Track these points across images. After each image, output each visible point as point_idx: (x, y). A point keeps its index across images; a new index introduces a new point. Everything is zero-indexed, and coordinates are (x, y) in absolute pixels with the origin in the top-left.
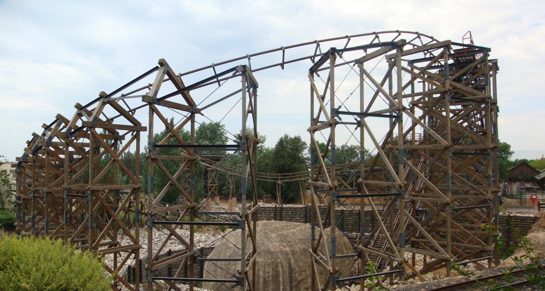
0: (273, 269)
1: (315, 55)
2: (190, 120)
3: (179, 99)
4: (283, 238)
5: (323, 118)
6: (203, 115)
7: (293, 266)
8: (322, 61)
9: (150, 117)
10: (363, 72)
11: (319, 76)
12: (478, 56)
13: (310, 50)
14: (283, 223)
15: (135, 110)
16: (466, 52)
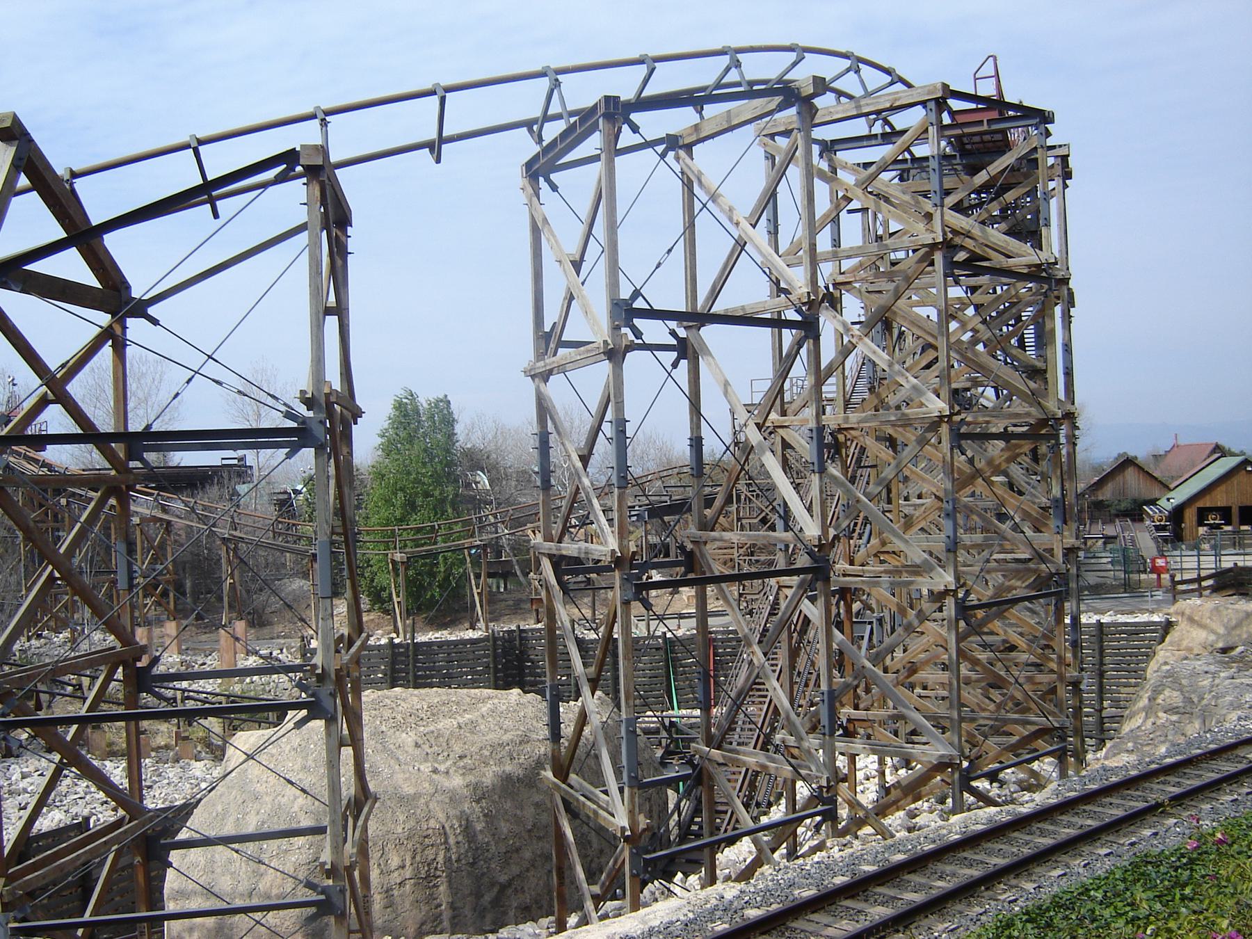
2: (110, 343)
4: (434, 745)
6: (155, 322)
8: (572, 137)
11: (554, 188)
14: (434, 695)
16: (985, 122)
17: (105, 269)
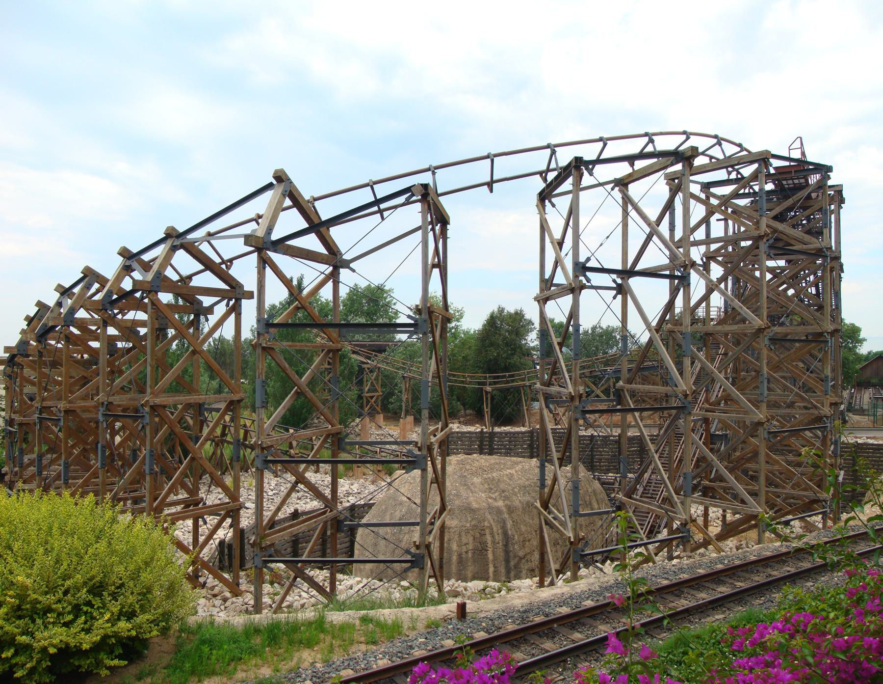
0: (474, 539)
1: (548, 170)
3: (311, 242)
4: (492, 485)
5: (560, 279)
6: (354, 271)
7: (510, 533)
9: (259, 273)
10: (627, 200)
11: (553, 205)
12: (814, 179)
13: (540, 160)
14: (494, 459)
15: (231, 261)
17: (329, 244)
